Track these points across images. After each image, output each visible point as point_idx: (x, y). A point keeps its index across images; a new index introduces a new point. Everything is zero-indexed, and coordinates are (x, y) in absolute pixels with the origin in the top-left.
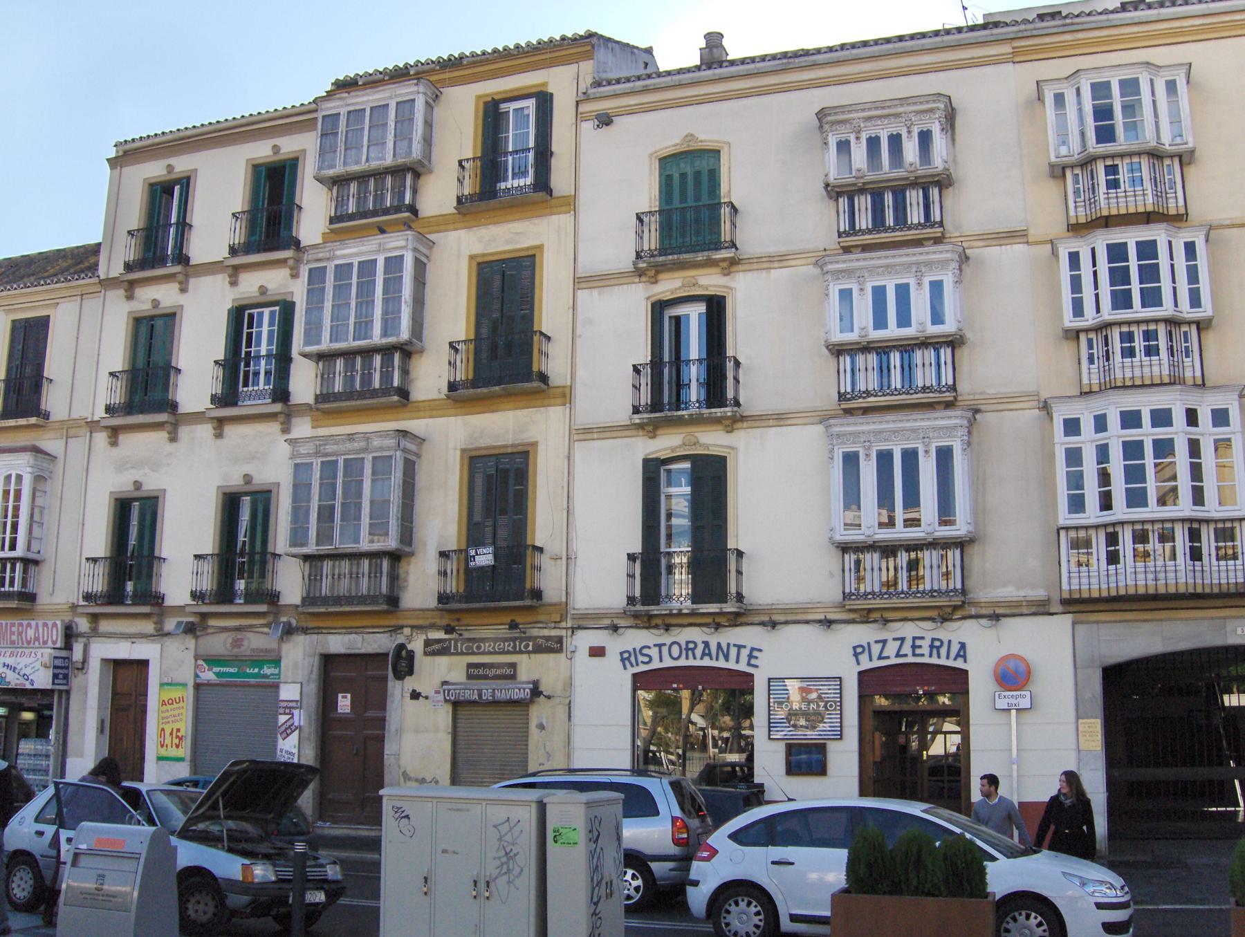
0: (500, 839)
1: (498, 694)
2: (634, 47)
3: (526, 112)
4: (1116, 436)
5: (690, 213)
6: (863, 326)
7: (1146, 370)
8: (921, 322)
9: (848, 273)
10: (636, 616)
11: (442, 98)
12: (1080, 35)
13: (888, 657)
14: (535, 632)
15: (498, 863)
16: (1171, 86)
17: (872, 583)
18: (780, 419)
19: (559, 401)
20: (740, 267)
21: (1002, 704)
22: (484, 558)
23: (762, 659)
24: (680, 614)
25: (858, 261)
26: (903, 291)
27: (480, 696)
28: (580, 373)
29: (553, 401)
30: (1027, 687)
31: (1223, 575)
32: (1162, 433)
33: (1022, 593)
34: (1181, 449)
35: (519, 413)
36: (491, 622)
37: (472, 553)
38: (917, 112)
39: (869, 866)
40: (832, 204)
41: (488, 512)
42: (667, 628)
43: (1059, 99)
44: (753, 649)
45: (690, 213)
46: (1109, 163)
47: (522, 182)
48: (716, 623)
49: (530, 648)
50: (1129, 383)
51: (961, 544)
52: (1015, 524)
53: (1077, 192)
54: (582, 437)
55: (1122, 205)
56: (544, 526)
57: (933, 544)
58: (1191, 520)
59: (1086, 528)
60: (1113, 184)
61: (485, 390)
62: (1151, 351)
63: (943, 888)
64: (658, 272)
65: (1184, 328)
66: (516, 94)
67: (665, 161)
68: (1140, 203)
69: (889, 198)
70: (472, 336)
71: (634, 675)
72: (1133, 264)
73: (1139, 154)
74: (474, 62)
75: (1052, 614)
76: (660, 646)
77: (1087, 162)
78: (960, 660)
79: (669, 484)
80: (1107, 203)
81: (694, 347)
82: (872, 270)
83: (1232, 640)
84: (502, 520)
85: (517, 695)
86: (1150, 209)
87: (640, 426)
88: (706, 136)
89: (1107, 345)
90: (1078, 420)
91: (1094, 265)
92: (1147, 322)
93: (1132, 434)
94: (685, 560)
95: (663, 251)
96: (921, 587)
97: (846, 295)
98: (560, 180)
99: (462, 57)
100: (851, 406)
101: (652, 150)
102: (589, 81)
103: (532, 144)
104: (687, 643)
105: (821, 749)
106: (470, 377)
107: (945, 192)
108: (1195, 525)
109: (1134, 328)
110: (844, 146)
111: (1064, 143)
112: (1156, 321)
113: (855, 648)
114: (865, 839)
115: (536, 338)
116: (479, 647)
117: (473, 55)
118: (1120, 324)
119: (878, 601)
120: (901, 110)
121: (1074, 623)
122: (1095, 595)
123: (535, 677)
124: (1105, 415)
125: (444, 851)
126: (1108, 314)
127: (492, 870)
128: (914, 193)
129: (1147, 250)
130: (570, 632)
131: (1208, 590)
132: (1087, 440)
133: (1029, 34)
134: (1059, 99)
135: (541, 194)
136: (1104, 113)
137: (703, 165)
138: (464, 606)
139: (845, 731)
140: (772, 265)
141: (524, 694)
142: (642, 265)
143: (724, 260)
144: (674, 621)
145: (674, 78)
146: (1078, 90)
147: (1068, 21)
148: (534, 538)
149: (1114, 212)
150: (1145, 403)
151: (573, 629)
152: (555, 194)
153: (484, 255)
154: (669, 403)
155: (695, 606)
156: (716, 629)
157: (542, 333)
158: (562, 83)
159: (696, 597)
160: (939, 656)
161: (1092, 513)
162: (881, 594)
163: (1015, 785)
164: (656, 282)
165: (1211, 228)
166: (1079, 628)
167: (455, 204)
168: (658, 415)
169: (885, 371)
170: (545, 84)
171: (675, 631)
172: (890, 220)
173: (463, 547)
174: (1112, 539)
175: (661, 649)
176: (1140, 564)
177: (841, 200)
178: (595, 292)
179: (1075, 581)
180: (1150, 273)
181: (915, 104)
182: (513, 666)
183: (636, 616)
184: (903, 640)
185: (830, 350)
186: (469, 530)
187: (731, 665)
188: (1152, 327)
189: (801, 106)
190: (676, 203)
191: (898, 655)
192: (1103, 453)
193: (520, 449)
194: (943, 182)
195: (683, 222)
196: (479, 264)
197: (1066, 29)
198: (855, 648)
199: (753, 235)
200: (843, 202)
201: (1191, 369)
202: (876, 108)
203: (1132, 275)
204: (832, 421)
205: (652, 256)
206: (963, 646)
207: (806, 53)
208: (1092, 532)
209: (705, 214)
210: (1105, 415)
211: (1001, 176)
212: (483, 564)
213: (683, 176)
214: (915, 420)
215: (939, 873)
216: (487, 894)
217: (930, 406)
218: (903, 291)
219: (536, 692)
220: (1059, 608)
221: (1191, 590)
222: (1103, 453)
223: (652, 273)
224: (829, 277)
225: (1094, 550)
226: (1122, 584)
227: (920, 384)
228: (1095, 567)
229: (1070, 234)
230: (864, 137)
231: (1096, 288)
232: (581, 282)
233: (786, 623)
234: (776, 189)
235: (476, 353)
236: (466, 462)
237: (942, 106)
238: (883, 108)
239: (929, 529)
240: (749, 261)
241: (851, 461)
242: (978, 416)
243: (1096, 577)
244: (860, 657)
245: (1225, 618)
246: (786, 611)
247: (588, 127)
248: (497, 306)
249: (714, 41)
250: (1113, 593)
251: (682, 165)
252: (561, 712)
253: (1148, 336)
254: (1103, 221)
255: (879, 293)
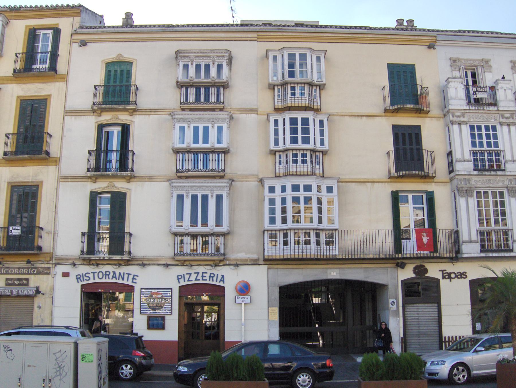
0: (56, 360)
1: (20, 292)
2: (96, 14)
3: (48, 35)
4: (289, 194)
5: (117, 88)
6: (188, 142)
7: (302, 169)
8: (213, 142)
9: (184, 119)
10: (84, 260)
11: (10, 24)
12: (284, 34)
13: (192, 281)
14: (38, 265)
15: (55, 370)
16: (318, 58)
17: (187, 249)
18: (150, 178)
19: (54, 164)
20: (137, 113)
21: (238, 301)
22: (17, 231)
23: (138, 280)
24: (104, 259)
25: (188, 115)
26: (206, 129)
27: (12, 293)
28: (64, 152)
29: (51, 163)
30: (249, 294)
31: (328, 251)
32: (308, 194)
33: (248, 256)
34: (315, 202)
35: (35, 168)
36: (17, 260)
37: (11, 228)
38: (217, 56)
39: (217, 369)
40: (178, 91)
41: (19, 211)
42: (98, 265)
43: (275, 58)
44: (134, 275)
45: (117, 88)
46: (293, 85)
47: (44, 66)
48: (119, 264)
49: (36, 272)
50: (295, 174)
51: (224, 235)
52: (245, 229)
53: (279, 96)
54: (63, 180)
55: (296, 103)
56: (44, 219)
57: (213, 234)
58: (317, 229)
59: (276, 230)
60: (293, 94)
61: (21, 156)
62: (304, 161)
63: (247, 377)
64: (101, 112)
65: (317, 154)
66: (44, 27)
67: (108, 64)
68: (303, 103)
69: (202, 90)
70: (16, 132)
71: (82, 285)
72: (300, 126)
73: (304, 83)
74: (26, 10)
75: (260, 265)
76: (94, 273)
77: (284, 84)
78: (114, 279)
79: (100, 204)
80: (290, 101)
81: (115, 144)
82: (193, 119)
83: (330, 277)
84: (25, 215)
85: (29, 293)
86: (307, 105)
87: (90, 177)
88: (127, 56)
89: (287, 158)
90: (274, 187)
91: (284, 125)
92: (303, 150)
93: (296, 194)
94: (107, 236)
95: (104, 102)
96: (207, 252)
97: (182, 129)
98: (61, 67)
99: (21, 7)
100: (181, 175)
101: (103, 59)
102: (78, 25)
103: (49, 50)
104: (106, 272)
105: (163, 318)
106: (14, 150)
107: (225, 90)
108: (318, 231)
109: (298, 152)
110: (186, 67)
111: (275, 76)
112: (307, 150)
113: (178, 276)
114: (215, 357)
115: (45, 135)
116: (12, 271)
117: (26, 7)
118: (293, 150)
119: (189, 257)
120: (211, 54)
121: (268, 269)
122: (278, 257)
123: (37, 285)
124: (285, 186)
125: (29, 366)
126: (288, 145)
127: (52, 374)
128: (213, 89)
129: (305, 121)
130: (54, 265)
131: (322, 257)
132: (278, 195)
133: (264, 30)
134: (275, 58)
135: (52, 72)
136: (291, 66)
137: (125, 68)
138: (7, 252)
139: (173, 311)
140: (151, 113)
141: (32, 292)
142: (95, 108)
143: (131, 109)
144: (101, 262)
145: (116, 29)
146: (283, 55)
147: (280, 28)
148: (39, 224)
149: (293, 105)
150: (302, 182)
151: (56, 265)
152: (58, 73)
153: (24, 97)
154: (103, 168)
155: (110, 256)
156: (97, 266)
157: (48, 134)
158: (66, 25)
159: (111, 252)
160: (213, 281)
161: (278, 225)
162: (190, 254)
163: (243, 334)
164: (100, 116)
165: (330, 115)
166: (270, 271)
167: (12, 72)
168: (98, 173)
169: (196, 161)
170: (58, 24)
171: (101, 267)
172: (202, 99)
173: (6, 226)
174: (286, 235)
175: (95, 275)
176: (297, 246)
177: (182, 89)
178: (73, 117)
179: (270, 252)
180: (306, 131)
181: (217, 53)
182: (27, 280)
183: (84, 260)
184: (198, 273)
185: (173, 150)
186: (9, 219)
187: (125, 282)
188: (305, 152)
189: (170, 48)
190: (112, 83)
191: (196, 280)
192: (284, 201)
193: (35, 184)
194: (225, 86)
195: (114, 91)
196: (21, 100)
197: (279, 31)
198: (178, 276)
199: (144, 99)
200: (183, 90)
201: (319, 170)
202: (201, 53)
203: (299, 130)
204: (173, 181)
205: (100, 104)
206: (223, 276)
207: (173, 26)
208: (278, 232)
209: (124, 88)
210: (285, 186)
211: (248, 86)
212: (16, 234)
213: (116, 71)
214: (208, 183)
215: (246, 371)
216: (49, 385)
217: (214, 177)
218: (206, 129)
219: (38, 292)
220: (262, 263)
221: (316, 257)
222: (284, 201)
223: (99, 112)
224: (175, 120)
225: (278, 240)
226: (289, 254)
227: (211, 168)
228: (278, 246)
229: (274, 112)
230: (194, 64)
231: (284, 134)
232: (68, 113)
233: (149, 265)
234: (155, 81)
235: (17, 140)
236: (10, 187)
237: (227, 55)
238: (203, 53)
239: (212, 228)
240: (141, 110)
241: (180, 198)
242: (233, 183)
243: (278, 250)
244: (180, 280)
245: (327, 268)
246: (148, 260)
247: (75, 46)
248: (28, 120)
249: (129, 16)
250: (285, 257)
251: (116, 67)
252: (49, 301)
253: (304, 155)
254: (305, 109)
255: (196, 129)
